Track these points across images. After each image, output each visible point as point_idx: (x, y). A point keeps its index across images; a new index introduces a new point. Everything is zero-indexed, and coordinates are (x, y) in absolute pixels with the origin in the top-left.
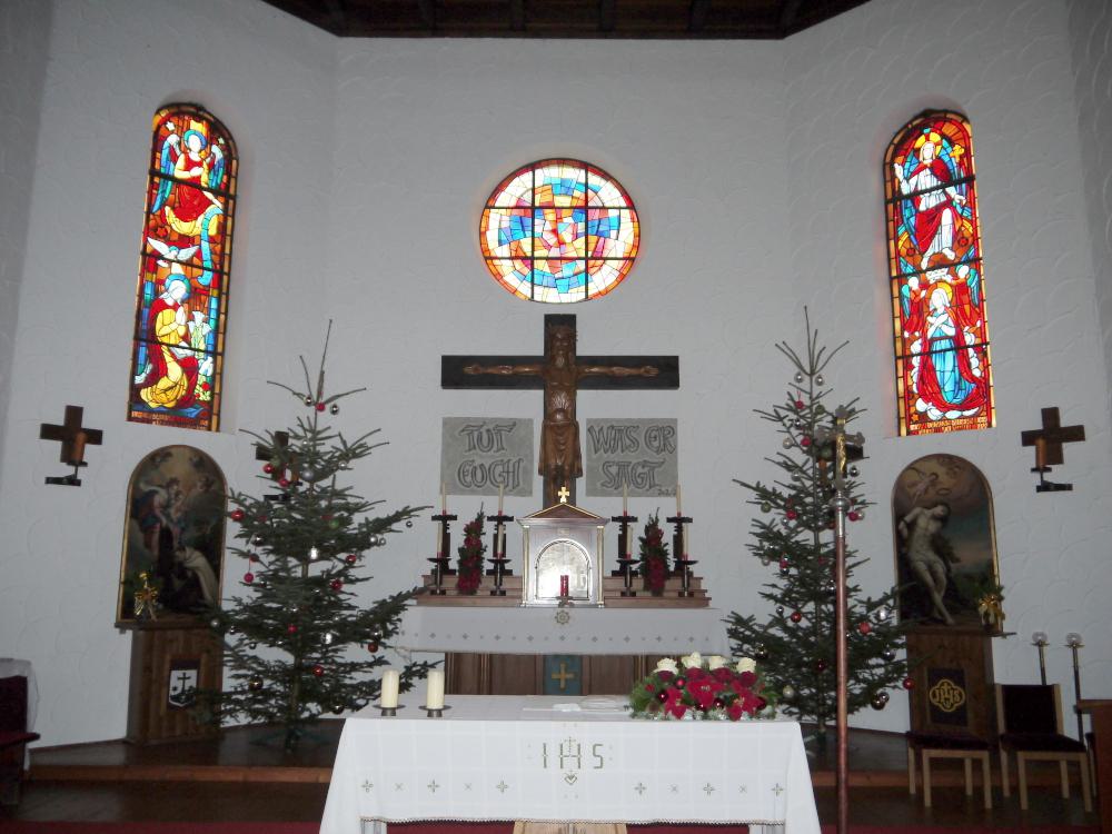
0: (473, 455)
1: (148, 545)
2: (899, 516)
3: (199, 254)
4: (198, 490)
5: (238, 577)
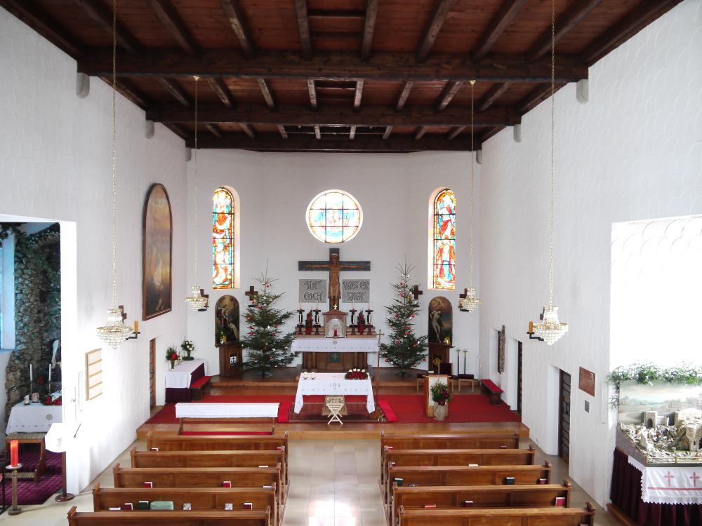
0: (308, 291)
1: (221, 324)
2: (430, 313)
3: (225, 235)
4: (232, 305)
5: (245, 330)
